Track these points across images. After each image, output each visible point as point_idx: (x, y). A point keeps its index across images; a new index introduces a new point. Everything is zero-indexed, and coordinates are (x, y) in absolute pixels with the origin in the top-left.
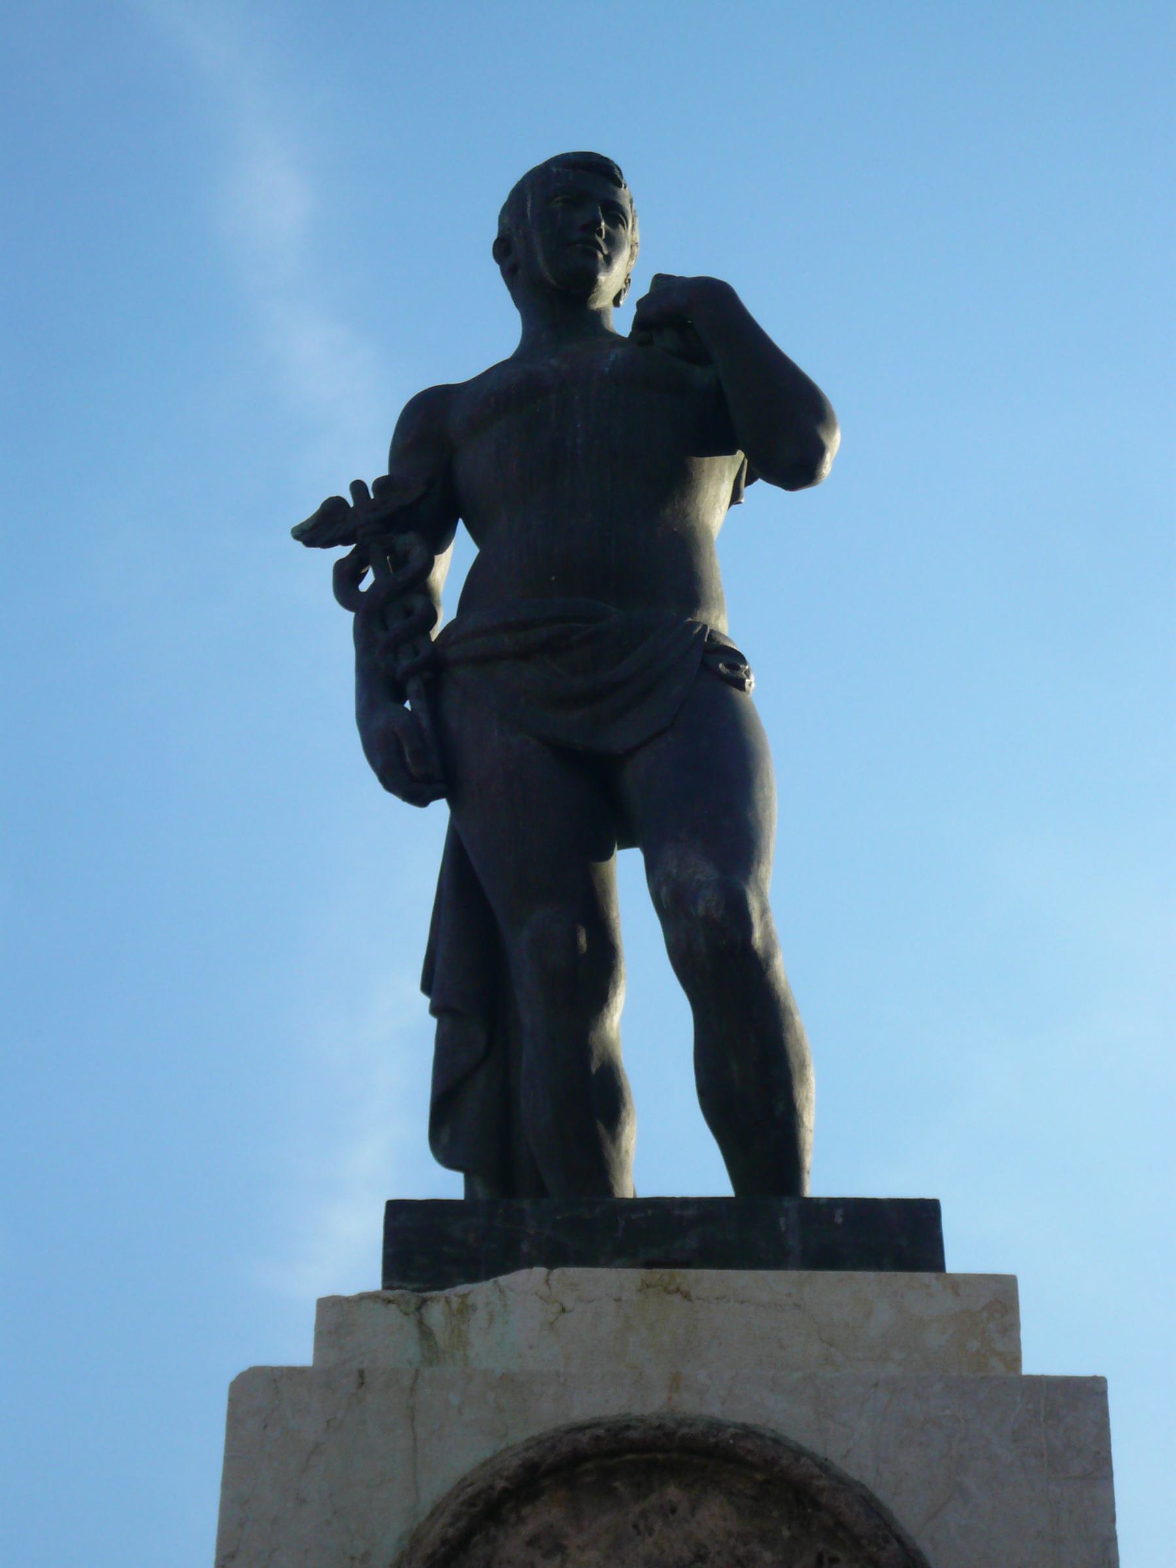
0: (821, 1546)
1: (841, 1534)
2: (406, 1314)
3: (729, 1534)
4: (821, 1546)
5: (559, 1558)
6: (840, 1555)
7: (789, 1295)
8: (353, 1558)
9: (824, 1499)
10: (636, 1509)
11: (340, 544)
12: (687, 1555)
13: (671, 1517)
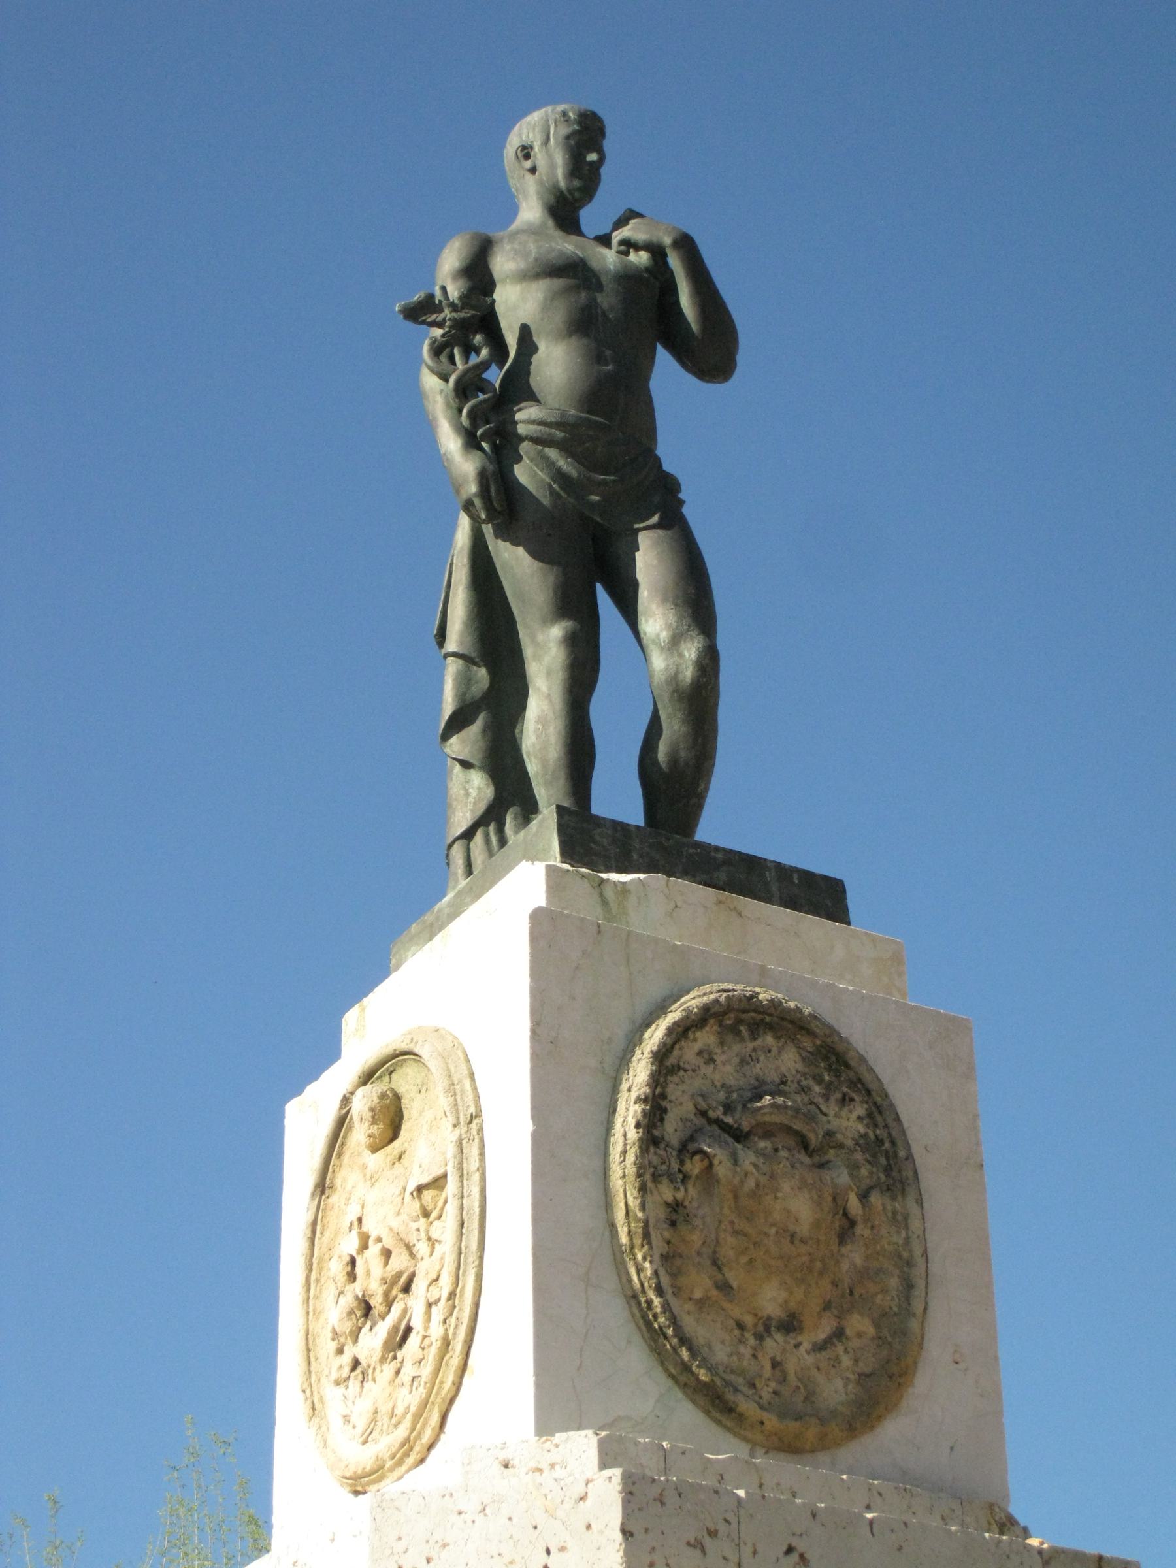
0: (845, 1090)
1: (859, 1086)
2: (594, 887)
3: (797, 1071)
4: (845, 1090)
5: (712, 1066)
6: (856, 1097)
7: (792, 926)
8: (603, 1041)
9: (852, 1063)
10: (751, 1045)
11: (528, 382)
12: (777, 1080)
13: (769, 1055)
